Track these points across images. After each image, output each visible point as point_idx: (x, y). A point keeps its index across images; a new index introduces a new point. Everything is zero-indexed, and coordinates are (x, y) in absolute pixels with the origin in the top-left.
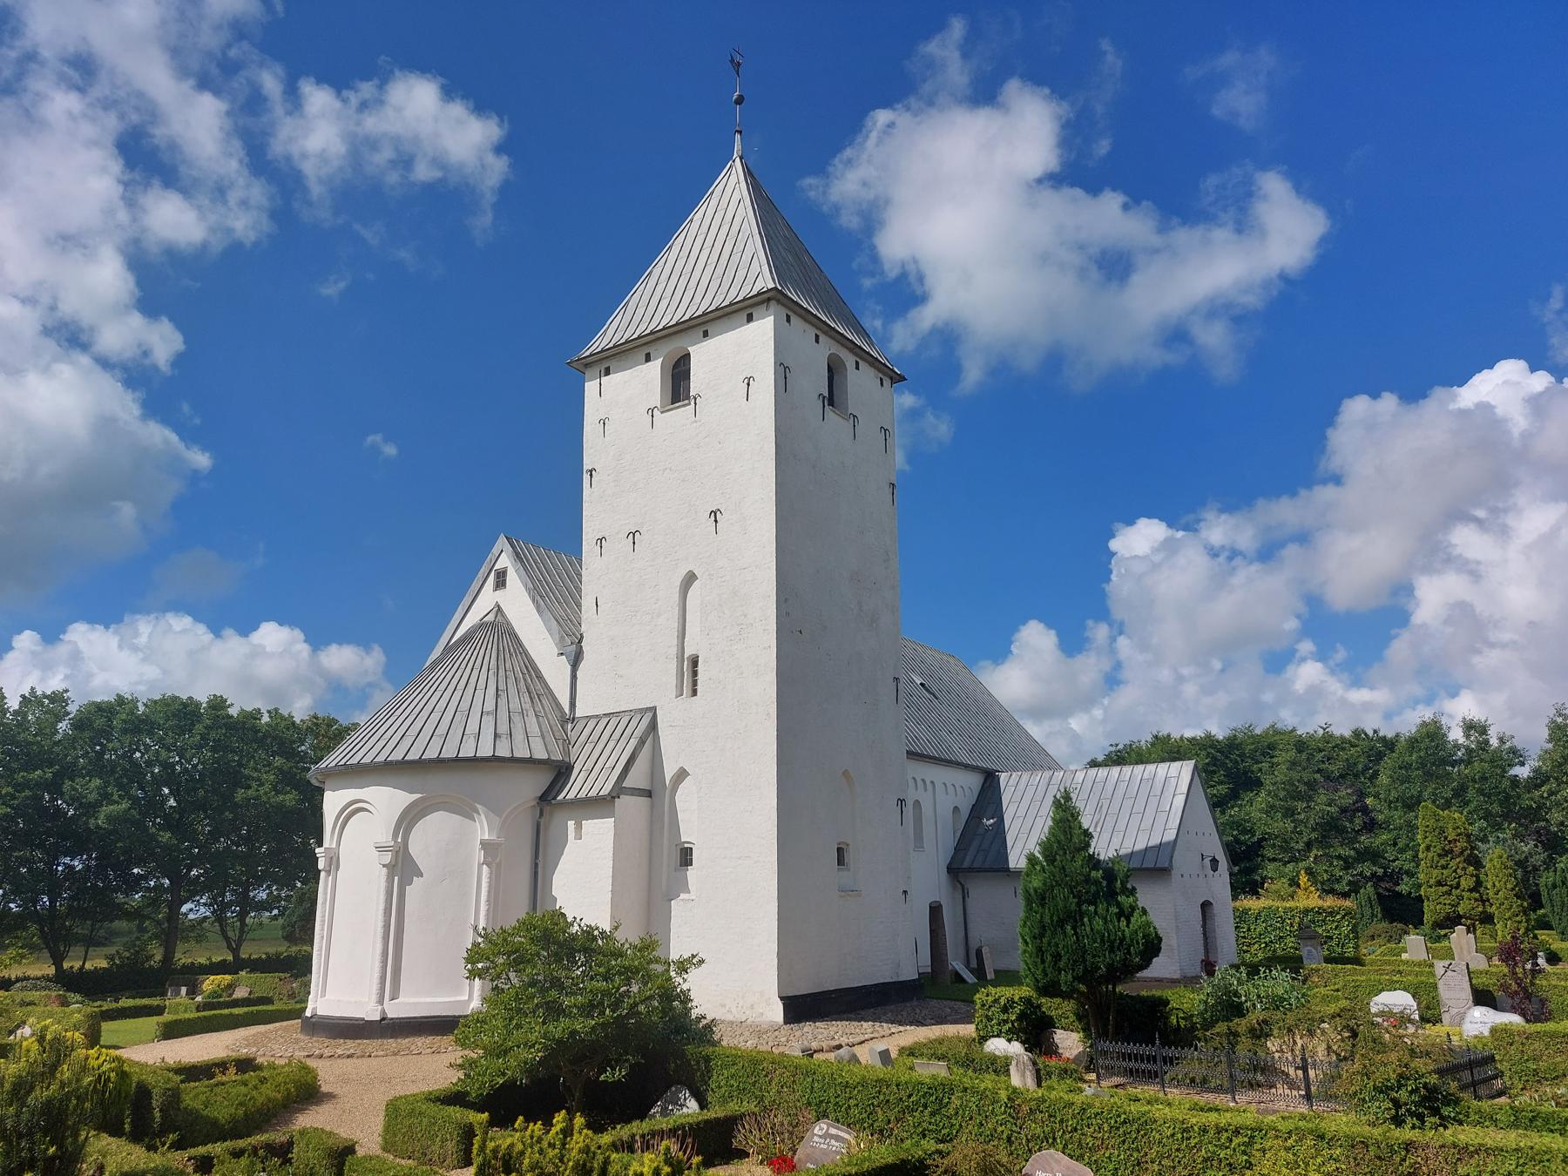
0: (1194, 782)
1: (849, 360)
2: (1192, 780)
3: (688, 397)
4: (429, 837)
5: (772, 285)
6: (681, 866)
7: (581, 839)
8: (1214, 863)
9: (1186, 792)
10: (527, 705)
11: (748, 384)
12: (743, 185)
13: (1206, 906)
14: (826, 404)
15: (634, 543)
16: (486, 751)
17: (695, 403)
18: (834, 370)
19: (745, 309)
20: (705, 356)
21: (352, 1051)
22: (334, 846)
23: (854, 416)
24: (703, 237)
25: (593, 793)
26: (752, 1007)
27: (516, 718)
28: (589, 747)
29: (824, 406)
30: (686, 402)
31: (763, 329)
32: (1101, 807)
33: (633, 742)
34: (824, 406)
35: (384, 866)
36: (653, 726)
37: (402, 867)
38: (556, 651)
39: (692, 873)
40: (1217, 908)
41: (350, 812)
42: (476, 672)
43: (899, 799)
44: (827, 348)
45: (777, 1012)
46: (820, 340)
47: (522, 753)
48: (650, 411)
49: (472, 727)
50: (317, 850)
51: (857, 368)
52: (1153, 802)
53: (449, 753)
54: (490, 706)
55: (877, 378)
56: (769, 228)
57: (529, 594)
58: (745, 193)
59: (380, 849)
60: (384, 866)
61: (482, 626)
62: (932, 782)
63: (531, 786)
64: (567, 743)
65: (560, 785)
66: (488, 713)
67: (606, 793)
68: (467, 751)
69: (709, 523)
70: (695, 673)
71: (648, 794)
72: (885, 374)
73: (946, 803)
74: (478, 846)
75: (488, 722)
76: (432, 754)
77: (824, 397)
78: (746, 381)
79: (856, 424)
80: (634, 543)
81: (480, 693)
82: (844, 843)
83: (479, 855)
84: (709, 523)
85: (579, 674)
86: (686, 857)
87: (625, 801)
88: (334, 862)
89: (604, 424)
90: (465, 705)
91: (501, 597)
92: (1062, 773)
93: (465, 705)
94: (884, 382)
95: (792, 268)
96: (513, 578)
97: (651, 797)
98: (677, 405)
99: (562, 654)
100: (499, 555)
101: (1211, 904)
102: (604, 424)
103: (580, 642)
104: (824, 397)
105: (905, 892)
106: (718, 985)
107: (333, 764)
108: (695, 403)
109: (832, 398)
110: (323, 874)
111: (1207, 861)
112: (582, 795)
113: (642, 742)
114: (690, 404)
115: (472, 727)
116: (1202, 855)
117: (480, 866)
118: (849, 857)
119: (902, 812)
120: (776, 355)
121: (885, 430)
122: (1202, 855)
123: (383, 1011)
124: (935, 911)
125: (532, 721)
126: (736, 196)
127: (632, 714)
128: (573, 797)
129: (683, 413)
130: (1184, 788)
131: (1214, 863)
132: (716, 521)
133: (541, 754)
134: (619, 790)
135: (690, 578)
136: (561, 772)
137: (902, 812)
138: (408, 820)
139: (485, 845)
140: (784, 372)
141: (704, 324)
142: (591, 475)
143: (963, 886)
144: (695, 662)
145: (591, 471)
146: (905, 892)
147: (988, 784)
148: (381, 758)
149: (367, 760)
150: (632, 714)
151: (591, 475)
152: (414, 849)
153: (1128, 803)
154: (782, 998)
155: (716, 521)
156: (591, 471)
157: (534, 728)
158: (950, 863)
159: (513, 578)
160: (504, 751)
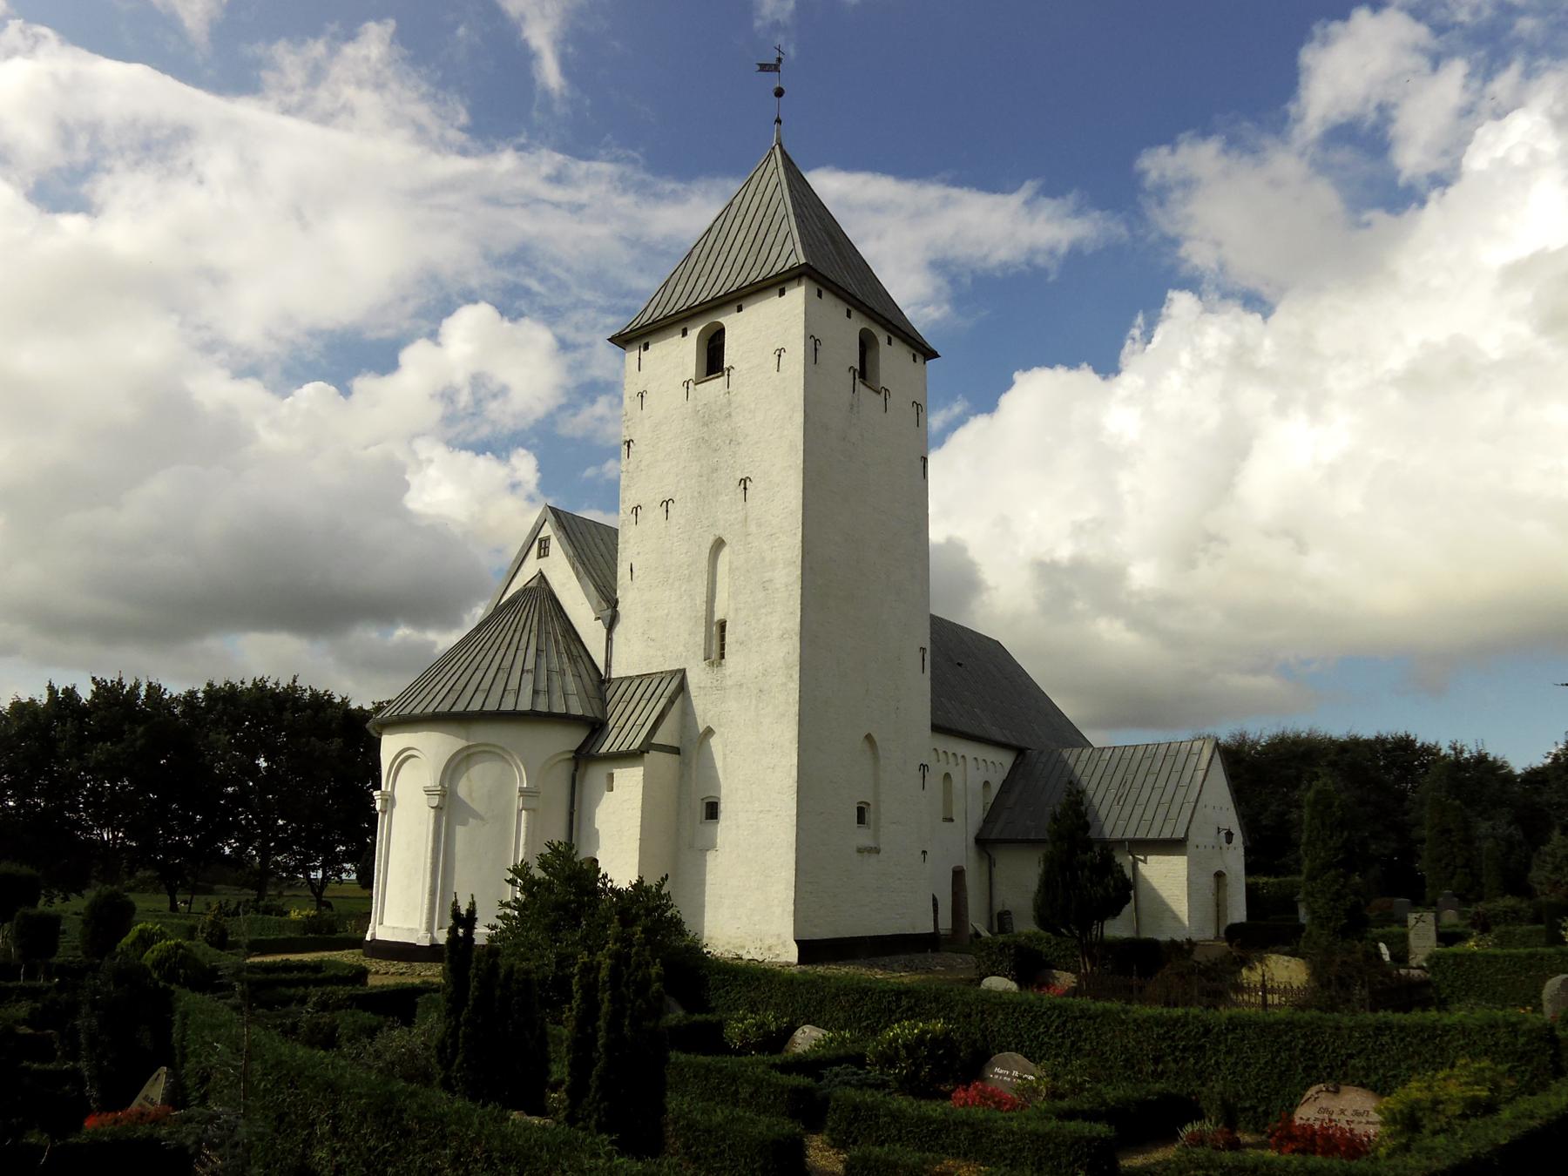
0: (1213, 761)
1: (882, 337)
2: (1212, 757)
3: (721, 369)
4: (474, 784)
5: (803, 261)
6: (707, 819)
7: (612, 790)
8: (1229, 836)
9: (1205, 767)
10: (566, 666)
11: (779, 356)
12: (781, 169)
13: (1219, 876)
14: (857, 377)
15: (667, 511)
16: (525, 705)
17: (728, 375)
18: (866, 344)
19: (777, 283)
20: (740, 328)
21: (404, 970)
22: (389, 789)
23: (886, 390)
24: (741, 218)
25: (624, 748)
26: (770, 948)
27: (556, 678)
28: (621, 706)
29: (855, 378)
30: (720, 373)
31: (797, 295)
32: (1126, 782)
33: (663, 701)
34: (855, 378)
35: (432, 807)
36: (682, 687)
37: (447, 806)
38: (593, 616)
39: (725, 828)
40: (1230, 878)
41: (404, 757)
42: (518, 635)
43: (922, 764)
44: (858, 323)
45: (791, 954)
46: (852, 316)
47: (559, 708)
48: (686, 384)
49: (513, 684)
50: (375, 793)
51: (890, 343)
52: (1174, 777)
53: (491, 706)
54: (530, 665)
55: (910, 353)
56: (804, 209)
57: (570, 561)
58: (783, 177)
59: (428, 791)
60: (432, 807)
61: (526, 591)
62: (963, 757)
63: (568, 740)
64: (604, 703)
65: (594, 739)
66: (528, 671)
67: (636, 748)
68: (508, 705)
69: (738, 491)
70: (723, 638)
71: (676, 751)
72: (917, 350)
73: (976, 777)
74: (518, 794)
75: (529, 678)
76: (475, 706)
77: (855, 371)
78: (778, 353)
79: (888, 397)
80: (667, 511)
81: (521, 654)
82: (865, 803)
83: (518, 802)
84: (738, 491)
85: (615, 636)
86: (712, 811)
87: (652, 757)
88: (390, 801)
89: (642, 396)
90: (506, 664)
91: (543, 563)
92: (1091, 750)
93: (506, 664)
94: (917, 357)
95: (825, 247)
96: (555, 546)
97: (679, 754)
98: (711, 377)
99: (599, 618)
100: (543, 525)
101: (1224, 874)
102: (642, 396)
103: (615, 607)
104: (855, 371)
105: (924, 852)
106: (738, 928)
107: (388, 715)
108: (728, 375)
109: (864, 372)
110: (380, 814)
111: (1223, 833)
112: (614, 749)
113: (671, 701)
114: (723, 375)
115: (513, 684)
116: (1219, 828)
117: (520, 812)
118: (870, 816)
119: (924, 777)
120: (806, 327)
121: (917, 405)
122: (1219, 828)
123: (433, 938)
124: (958, 874)
125: (569, 678)
126: (774, 180)
127: (664, 675)
128: (605, 751)
129: (717, 384)
130: (1204, 764)
131: (1229, 836)
132: (745, 488)
133: (577, 709)
134: (647, 747)
135: (719, 544)
136: (596, 727)
137: (924, 777)
138: (454, 767)
139: (521, 790)
140: (814, 344)
141: (736, 299)
142: (629, 446)
143: (990, 856)
144: (722, 626)
145: (629, 442)
146: (924, 852)
147: (1018, 762)
148: (430, 709)
149: (418, 711)
150: (664, 675)
151: (629, 446)
152: (462, 789)
153: (1151, 779)
154: (796, 941)
155: (745, 488)
156: (629, 442)
157: (572, 686)
158: (978, 835)
159: (555, 546)
160: (542, 707)
